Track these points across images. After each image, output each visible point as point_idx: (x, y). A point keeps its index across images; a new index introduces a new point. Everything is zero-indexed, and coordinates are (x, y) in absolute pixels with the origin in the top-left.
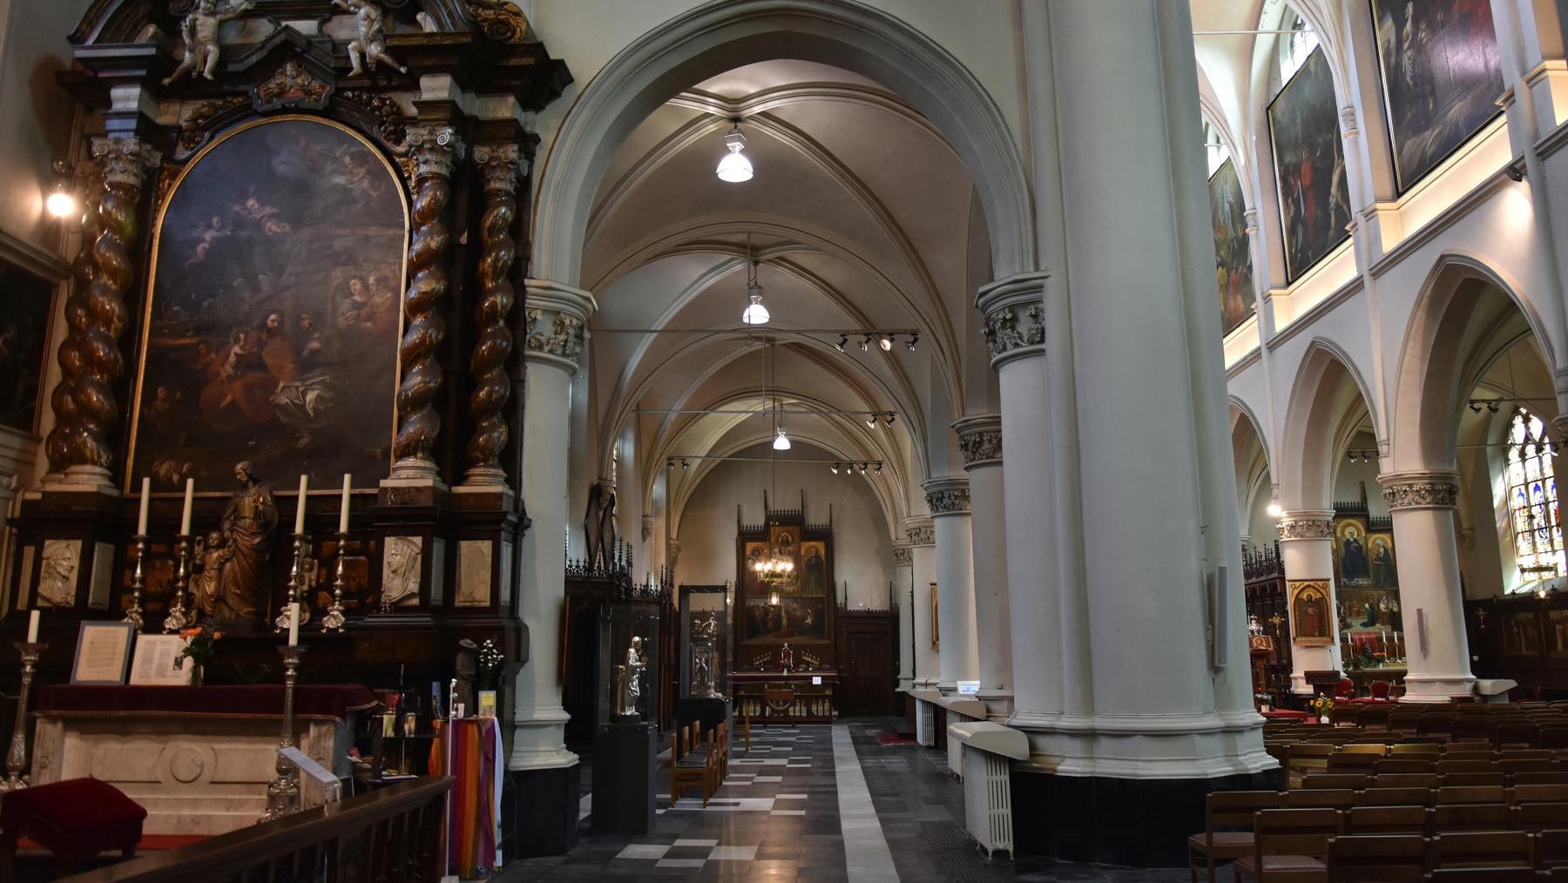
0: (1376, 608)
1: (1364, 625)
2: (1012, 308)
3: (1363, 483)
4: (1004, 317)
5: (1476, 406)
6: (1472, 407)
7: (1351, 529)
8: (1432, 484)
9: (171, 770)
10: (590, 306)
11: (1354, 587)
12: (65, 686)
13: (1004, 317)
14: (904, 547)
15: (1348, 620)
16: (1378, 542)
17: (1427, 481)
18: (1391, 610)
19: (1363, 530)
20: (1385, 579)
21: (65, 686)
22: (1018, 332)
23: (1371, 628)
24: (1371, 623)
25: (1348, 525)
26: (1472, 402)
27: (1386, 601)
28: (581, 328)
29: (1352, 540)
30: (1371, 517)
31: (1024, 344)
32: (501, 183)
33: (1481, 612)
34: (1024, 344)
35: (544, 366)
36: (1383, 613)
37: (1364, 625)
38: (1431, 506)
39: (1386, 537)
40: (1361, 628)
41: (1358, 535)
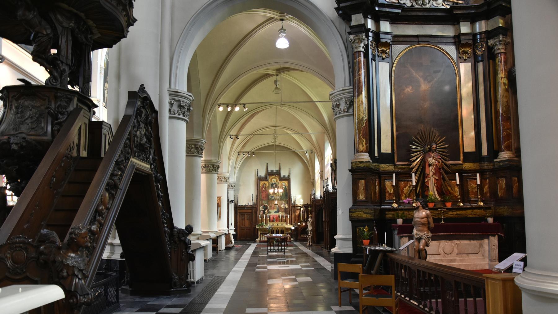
0: (280, 206)
1: (275, 212)
2: (338, 100)
3: (280, 163)
4: (337, 104)
5: (232, 137)
6: (230, 137)
7: (273, 180)
8: (205, 165)
9: (444, 252)
10: (191, 98)
11: (273, 199)
12: (410, 224)
13: (337, 104)
14: (231, 184)
15: (270, 211)
16: (283, 184)
17: (204, 163)
18: (285, 207)
19: (278, 180)
20: (284, 197)
21: (410, 224)
22: (340, 109)
23: (278, 213)
24: (278, 211)
25: (273, 178)
26: (231, 136)
27: (284, 204)
28: (189, 106)
29: (274, 183)
30: (281, 175)
31: (342, 112)
32: (500, 48)
33: (310, 208)
34: (342, 112)
35: (180, 121)
36: (282, 208)
37: (275, 212)
38: (205, 172)
39: (455, 181)
40: (274, 213)
41: (276, 181)
